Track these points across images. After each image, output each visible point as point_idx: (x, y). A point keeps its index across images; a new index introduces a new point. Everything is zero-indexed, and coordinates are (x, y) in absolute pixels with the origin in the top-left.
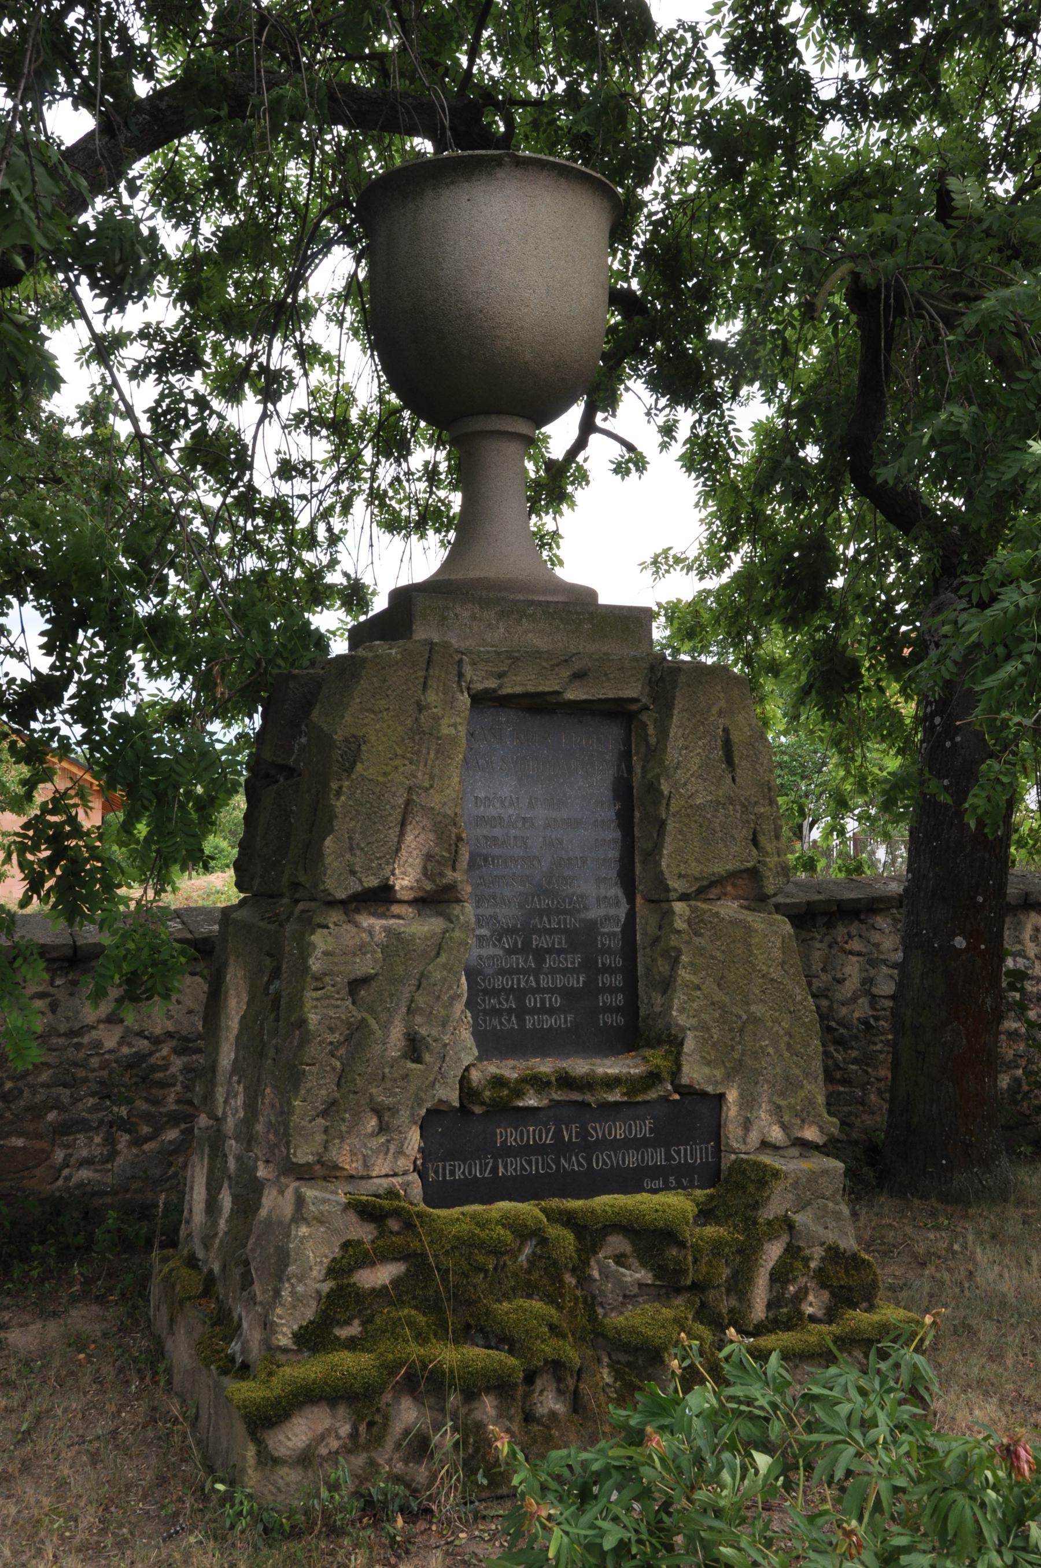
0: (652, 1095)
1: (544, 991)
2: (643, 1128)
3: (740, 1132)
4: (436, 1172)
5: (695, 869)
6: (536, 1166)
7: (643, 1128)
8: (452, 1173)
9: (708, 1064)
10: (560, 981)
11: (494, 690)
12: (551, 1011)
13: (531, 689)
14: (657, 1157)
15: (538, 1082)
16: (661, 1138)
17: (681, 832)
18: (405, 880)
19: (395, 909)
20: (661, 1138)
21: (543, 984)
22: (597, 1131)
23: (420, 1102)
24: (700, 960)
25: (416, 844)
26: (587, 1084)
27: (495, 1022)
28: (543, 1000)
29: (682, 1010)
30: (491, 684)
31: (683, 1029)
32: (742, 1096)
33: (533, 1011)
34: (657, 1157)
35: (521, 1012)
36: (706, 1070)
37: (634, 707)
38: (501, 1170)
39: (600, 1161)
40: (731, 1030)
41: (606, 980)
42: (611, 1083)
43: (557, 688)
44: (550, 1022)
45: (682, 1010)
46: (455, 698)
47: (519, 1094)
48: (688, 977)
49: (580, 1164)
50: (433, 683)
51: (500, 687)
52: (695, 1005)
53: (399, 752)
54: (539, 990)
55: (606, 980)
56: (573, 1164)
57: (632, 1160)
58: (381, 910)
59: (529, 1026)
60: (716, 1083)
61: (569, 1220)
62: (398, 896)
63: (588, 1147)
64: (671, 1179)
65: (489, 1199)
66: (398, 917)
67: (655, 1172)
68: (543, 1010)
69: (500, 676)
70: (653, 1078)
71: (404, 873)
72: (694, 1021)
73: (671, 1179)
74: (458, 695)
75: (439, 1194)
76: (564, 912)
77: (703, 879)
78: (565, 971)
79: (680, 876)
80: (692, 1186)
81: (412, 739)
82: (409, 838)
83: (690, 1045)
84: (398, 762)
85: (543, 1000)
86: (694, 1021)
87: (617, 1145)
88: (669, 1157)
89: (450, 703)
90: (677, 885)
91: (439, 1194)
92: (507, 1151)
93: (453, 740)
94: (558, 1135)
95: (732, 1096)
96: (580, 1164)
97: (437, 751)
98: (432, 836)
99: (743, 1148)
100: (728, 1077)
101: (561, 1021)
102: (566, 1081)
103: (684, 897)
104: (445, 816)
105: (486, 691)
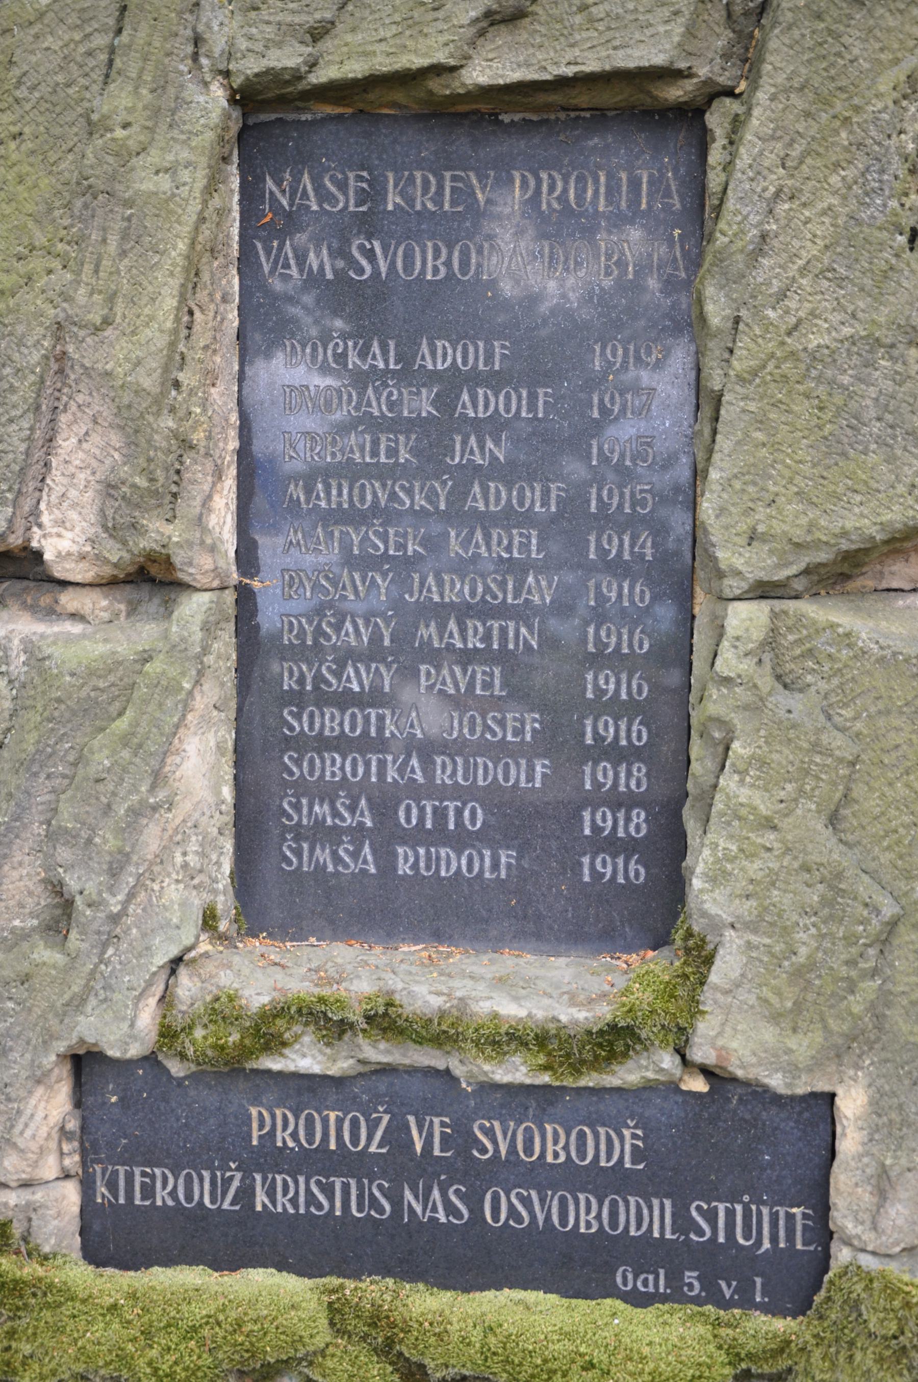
0: (628, 1074)
1: (443, 792)
2: (622, 1146)
3: (866, 1197)
4: (112, 1186)
5: (792, 520)
6: (342, 1199)
7: (622, 1146)
8: (148, 1191)
9: (775, 1018)
10: (485, 773)
11: (297, 76)
12: (460, 840)
13: (384, 64)
14: (656, 1219)
15: (329, 1023)
16: (658, 1174)
17: (761, 422)
18: (65, 537)
19: (69, 600)
20: (658, 1174)
21: (441, 777)
22: (495, 1138)
23: (49, 1037)
24: (782, 756)
25: (82, 458)
26: (442, 1033)
27: (323, 855)
28: (440, 815)
29: (716, 878)
30: (288, 57)
31: (717, 926)
32: (876, 1106)
33: (417, 837)
34: (656, 1219)
35: (387, 836)
36: (769, 1034)
37: (675, 93)
38: (261, 1198)
39: (505, 1207)
40: (850, 940)
41: (602, 775)
42: (503, 1039)
43: (441, 57)
44: (451, 862)
45: (716, 878)
46: (181, 102)
47: (274, 1043)
48: (744, 794)
49: (450, 1209)
50: (129, 64)
51: (313, 65)
52: (754, 868)
53: (40, 239)
54: (432, 790)
55: (602, 775)
56: (437, 1206)
57: (586, 1215)
58: (45, 600)
59: (403, 869)
60: (793, 1070)
61: (390, 1342)
62: (58, 573)
63: (474, 1174)
64: (690, 1276)
65: (227, 1261)
66: (75, 616)
67: (645, 1253)
68: (438, 835)
69: (318, 33)
70: (615, 1040)
71: (61, 523)
72: (747, 908)
73: (690, 1276)
74: (192, 91)
75: (110, 1239)
76: (503, 611)
77: (818, 544)
78: (500, 751)
79: (753, 537)
80: (746, 1302)
81: (68, 206)
82: (66, 443)
83: (726, 967)
84: (37, 263)
85: (440, 815)
86: (747, 908)
87: (540, 1176)
88: (683, 1223)
89: (165, 112)
90: (737, 559)
91: (110, 1239)
92: (270, 1158)
93: (165, 206)
94: (397, 1137)
95: (852, 1104)
96: (450, 1209)
97: (125, 236)
98: (116, 439)
99: (870, 1239)
100: (839, 1053)
101: (495, 863)
102: (385, 1021)
103: (764, 591)
104: (139, 391)
105: (272, 76)
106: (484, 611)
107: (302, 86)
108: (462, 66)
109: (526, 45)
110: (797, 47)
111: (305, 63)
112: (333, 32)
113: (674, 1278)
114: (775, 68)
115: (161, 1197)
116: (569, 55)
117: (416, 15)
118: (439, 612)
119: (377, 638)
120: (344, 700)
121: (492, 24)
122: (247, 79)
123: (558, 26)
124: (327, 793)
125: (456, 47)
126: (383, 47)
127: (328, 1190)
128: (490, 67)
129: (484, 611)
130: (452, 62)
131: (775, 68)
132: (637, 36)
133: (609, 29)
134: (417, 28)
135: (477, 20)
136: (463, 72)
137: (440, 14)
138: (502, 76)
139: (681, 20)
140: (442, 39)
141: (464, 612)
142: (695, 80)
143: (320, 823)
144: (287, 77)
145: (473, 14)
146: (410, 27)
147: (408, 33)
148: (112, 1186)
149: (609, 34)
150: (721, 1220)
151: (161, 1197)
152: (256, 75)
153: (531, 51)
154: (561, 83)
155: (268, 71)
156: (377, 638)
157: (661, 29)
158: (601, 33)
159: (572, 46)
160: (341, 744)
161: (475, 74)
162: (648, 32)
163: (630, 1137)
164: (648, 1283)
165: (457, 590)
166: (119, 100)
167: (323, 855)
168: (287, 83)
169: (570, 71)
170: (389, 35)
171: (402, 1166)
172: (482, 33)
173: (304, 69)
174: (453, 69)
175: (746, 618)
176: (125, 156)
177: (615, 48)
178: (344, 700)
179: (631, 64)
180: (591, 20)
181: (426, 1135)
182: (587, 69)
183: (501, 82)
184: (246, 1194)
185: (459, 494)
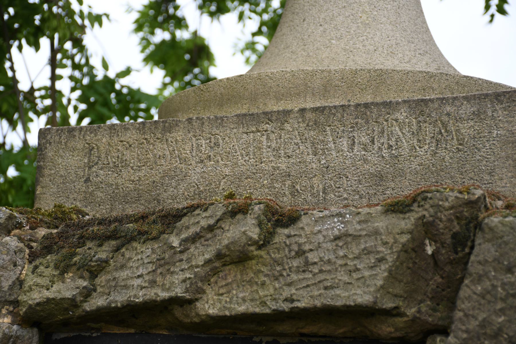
11: (73, 303)
43: (179, 291)
107: (79, 312)
108: (197, 300)
109: (250, 282)
110: (488, 297)
111: (80, 293)
112: (108, 269)
114: (466, 315)
116: (287, 293)
117: (167, 256)
121: (224, 265)
122: (30, 306)
123: (278, 268)
125: (191, 284)
126: (139, 281)
128: (220, 301)
130: (187, 296)
131: (466, 315)
132: (346, 278)
133: (321, 271)
134: (167, 267)
135: (208, 262)
136: (198, 304)
137: (184, 257)
138: (229, 309)
139: (384, 266)
140: (181, 277)
142: (405, 319)
144: (66, 306)
145: (207, 256)
146: (161, 266)
147: (159, 271)
149: (322, 277)
152: (38, 304)
153: (255, 288)
154: (278, 316)
155: (49, 301)
157: (367, 273)
158: (314, 275)
159: (290, 285)
161: (207, 306)
162: (355, 275)
168: (67, 310)
169: (286, 307)
170: (145, 272)
172: (215, 272)
173: (79, 299)
174: (190, 302)
177: (326, 288)
179: (339, 303)
180: (307, 263)
182: (301, 305)
183: (227, 313)
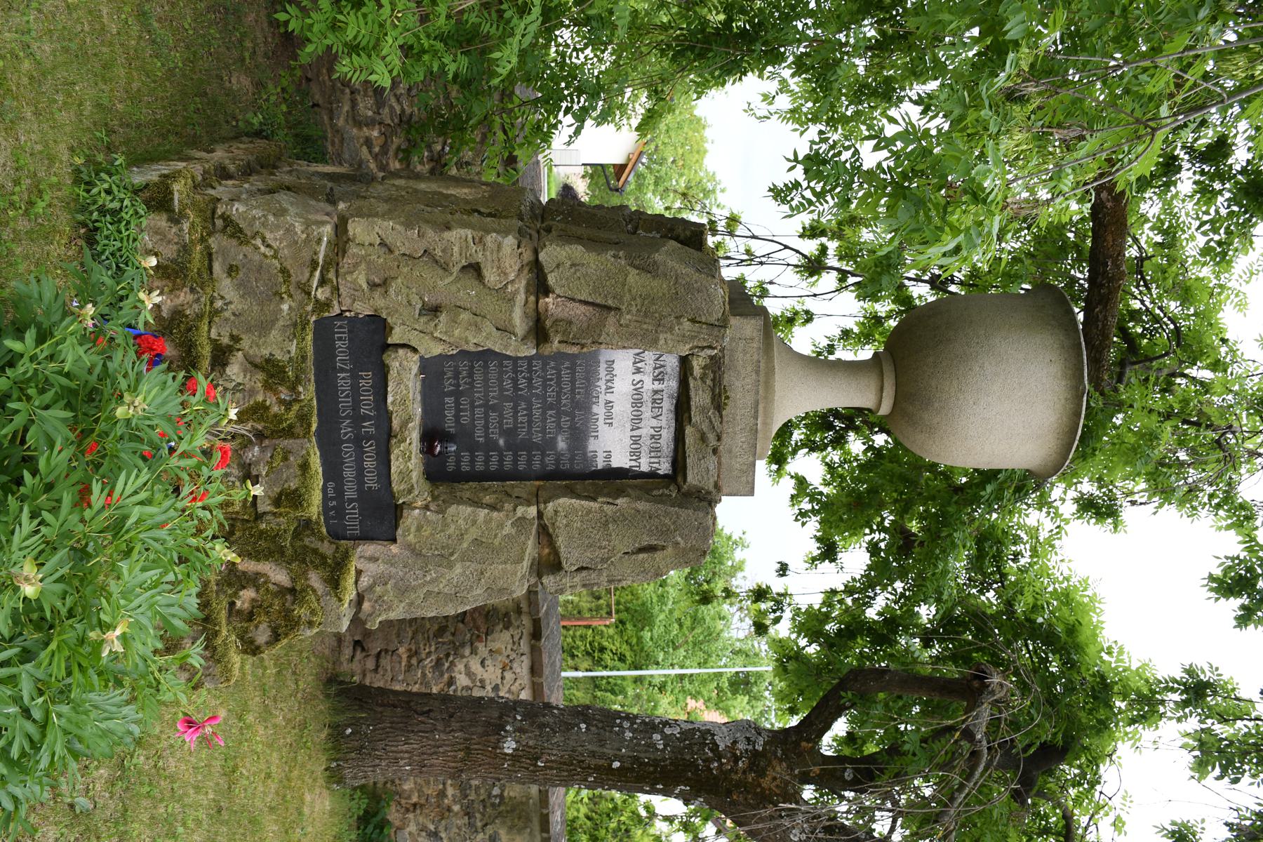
3: (368, 554)
4: (340, 327)
5: (561, 522)
6: (345, 402)
8: (340, 339)
10: (480, 423)
14: (350, 492)
16: (364, 496)
24: (493, 525)
28: (465, 410)
33: (457, 403)
34: (350, 492)
35: (457, 394)
38: (342, 375)
39: (348, 449)
41: (480, 457)
49: (346, 434)
51: (695, 379)
54: (473, 407)
56: (346, 429)
57: (349, 473)
59: (447, 400)
64: (334, 503)
67: (340, 492)
68: (458, 410)
76: (530, 427)
94: (366, 418)
95: (394, 549)
96: (346, 434)
103: (540, 515)
106: (530, 422)
113: (332, 499)
115: (338, 343)
118: (529, 408)
119: (521, 390)
120: (500, 380)
124: (471, 375)
127: (347, 396)
129: (530, 422)
141: (530, 415)
143: (460, 373)
148: (340, 327)
150: (353, 511)
151: (338, 343)
154: (684, 452)
156: (521, 390)
160: (486, 380)
163: (375, 486)
164: (331, 493)
165: (537, 414)
166: (687, 325)
167: (449, 374)
171: (357, 419)
175: (532, 511)
176: (671, 329)
178: (500, 380)
181: (368, 427)
184: (342, 370)
185: (566, 414)
